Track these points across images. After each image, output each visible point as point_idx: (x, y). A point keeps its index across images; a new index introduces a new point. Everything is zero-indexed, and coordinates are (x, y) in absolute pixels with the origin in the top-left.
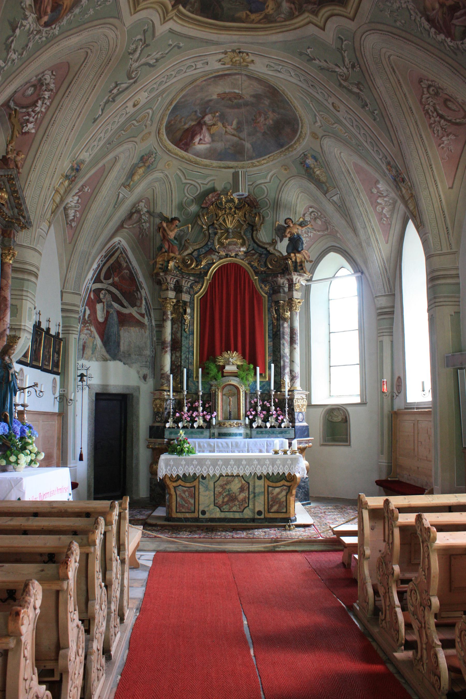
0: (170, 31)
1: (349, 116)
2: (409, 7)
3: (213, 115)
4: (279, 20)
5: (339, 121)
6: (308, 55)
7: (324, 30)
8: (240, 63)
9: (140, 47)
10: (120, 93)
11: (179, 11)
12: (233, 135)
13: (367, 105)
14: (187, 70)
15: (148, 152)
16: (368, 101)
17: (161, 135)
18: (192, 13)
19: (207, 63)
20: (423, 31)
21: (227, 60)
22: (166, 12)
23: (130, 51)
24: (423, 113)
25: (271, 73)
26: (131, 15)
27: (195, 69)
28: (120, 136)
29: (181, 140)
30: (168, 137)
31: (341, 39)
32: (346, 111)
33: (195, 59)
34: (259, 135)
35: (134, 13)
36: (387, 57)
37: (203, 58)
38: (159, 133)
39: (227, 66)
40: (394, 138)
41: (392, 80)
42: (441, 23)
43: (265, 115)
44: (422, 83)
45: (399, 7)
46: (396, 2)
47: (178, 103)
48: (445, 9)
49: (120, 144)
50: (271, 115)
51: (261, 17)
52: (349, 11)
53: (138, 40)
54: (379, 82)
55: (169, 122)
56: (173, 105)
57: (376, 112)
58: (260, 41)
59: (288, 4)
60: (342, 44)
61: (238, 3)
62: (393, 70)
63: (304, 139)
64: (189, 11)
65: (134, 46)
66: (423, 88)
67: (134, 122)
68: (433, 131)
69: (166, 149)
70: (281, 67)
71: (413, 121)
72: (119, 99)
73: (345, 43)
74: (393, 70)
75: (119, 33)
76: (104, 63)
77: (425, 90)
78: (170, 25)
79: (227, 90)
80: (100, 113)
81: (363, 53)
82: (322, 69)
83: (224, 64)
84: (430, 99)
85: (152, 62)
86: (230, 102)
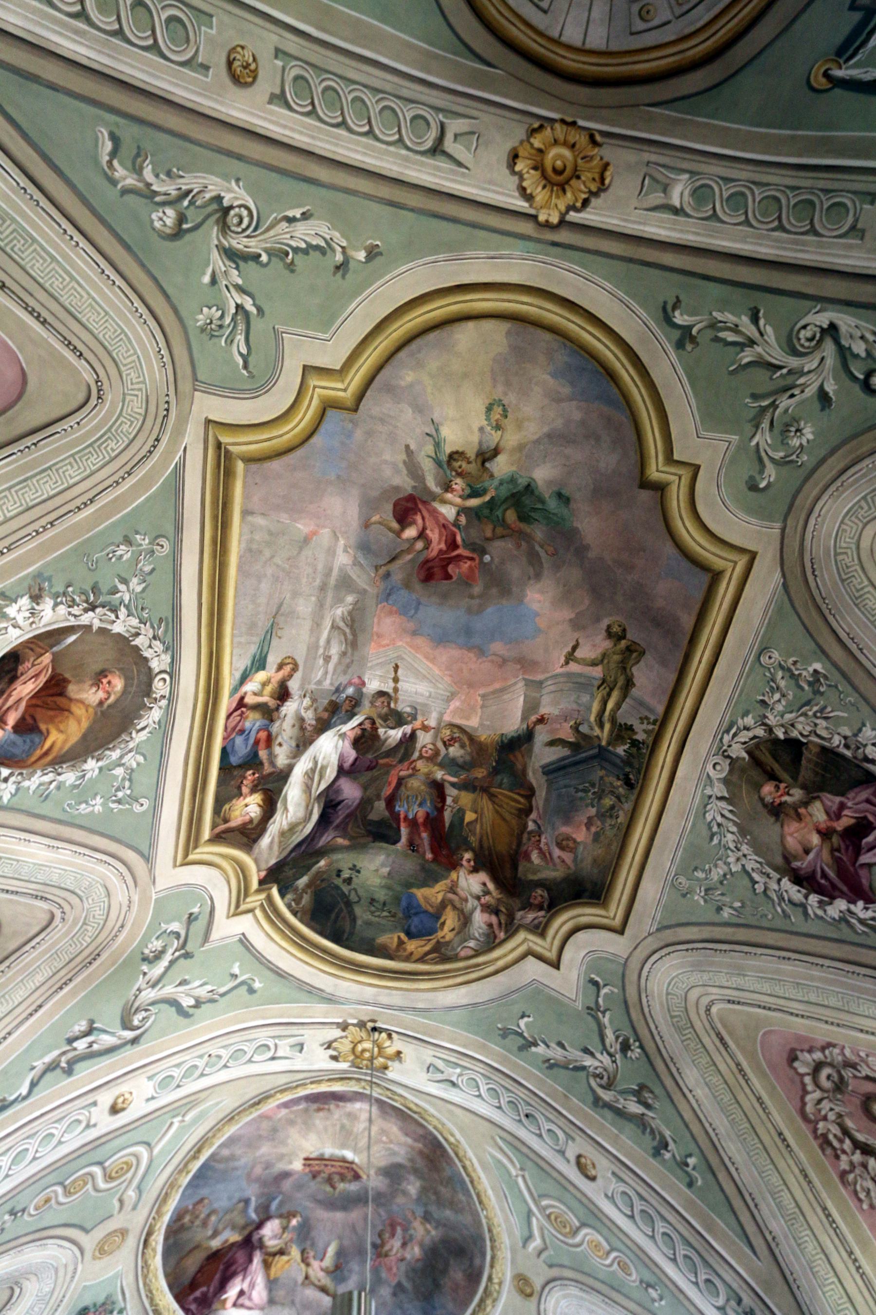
0: (240, 941)
1: (622, 1188)
2: (749, 868)
3: (285, 1221)
4: (463, 954)
5: (593, 1217)
6: (521, 1035)
7: (556, 965)
8: (372, 1059)
9: (171, 951)
10: (90, 1055)
11: (269, 899)
12: (323, 1290)
13: (666, 1146)
14: (256, 1058)
15: (101, 1299)
16: (667, 1133)
17: (149, 1251)
18: (295, 914)
19: (301, 1047)
20: (788, 909)
21: (345, 1047)
22: (244, 892)
23: (146, 951)
24: (815, 1144)
25: (434, 1089)
26: (175, 866)
27: (273, 1058)
28: (47, 1201)
29: (193, 1285)
30: (165, 1265)
31: (596, 984)
32: (614, 1173)
33: (277, 1031)
34: (385, 1292)
35: (182, 865)
36: (702, 1011)
37: (294, 1030)
38: (146, 1242)
39: (344, 1066)
40: (751, 1229)
41: (722, 1067)
42: (832, 874)
43: (405, 1229)
44: (796, 1064)
45: (725, 875)
46: (716, 866)
47: (213, 1157)
48: (835, 840)
49: (40, 1235)
50: (419, 1230)
51: (427, 948)
52: (612, 915)
53: (172, 932)
54: (691, 1077)
55: (178, 1217)
56: (203, 1158)
57: (691, 1161)
58: (420, 1005)
59: (486, 917)
60: (598, 996)
61: (385, 914)
62: (722, 1039)
63: (495, 1300)
64: (289, 906)
65: (157, 945)
66: (802, 1076)
67: (97, 1170)
68: (856, 1193)
69: (152, 1304)
70: (458, 1070)
71: (797, 1171)
72: (83, 1070)
73: (604, 991)
74: (722, 1039)
75: (136, 898)
76: (79, 959)
77: (808, 1080)
78: (245, 925)
79: (329, 1151)
80: (24, 1091)
81: (646, 1010)
82: (551, 1065)
83: (335, 1058)
84: (826, 1105)
85: (187, 1002)
86: (328, 1189)
